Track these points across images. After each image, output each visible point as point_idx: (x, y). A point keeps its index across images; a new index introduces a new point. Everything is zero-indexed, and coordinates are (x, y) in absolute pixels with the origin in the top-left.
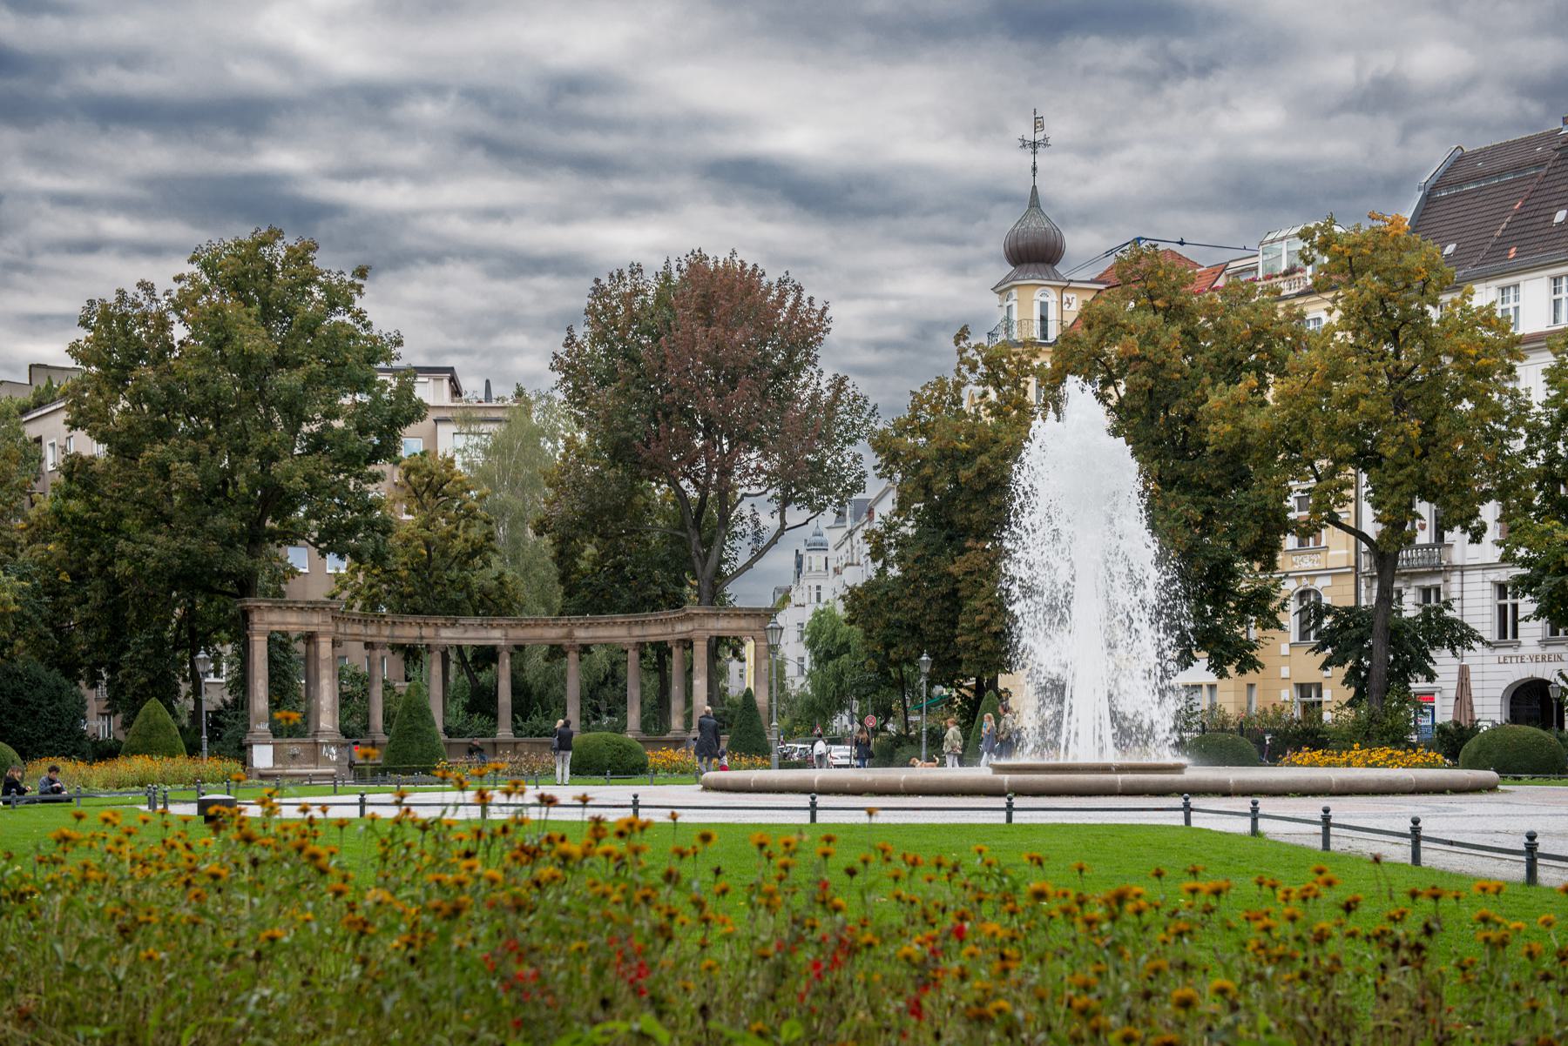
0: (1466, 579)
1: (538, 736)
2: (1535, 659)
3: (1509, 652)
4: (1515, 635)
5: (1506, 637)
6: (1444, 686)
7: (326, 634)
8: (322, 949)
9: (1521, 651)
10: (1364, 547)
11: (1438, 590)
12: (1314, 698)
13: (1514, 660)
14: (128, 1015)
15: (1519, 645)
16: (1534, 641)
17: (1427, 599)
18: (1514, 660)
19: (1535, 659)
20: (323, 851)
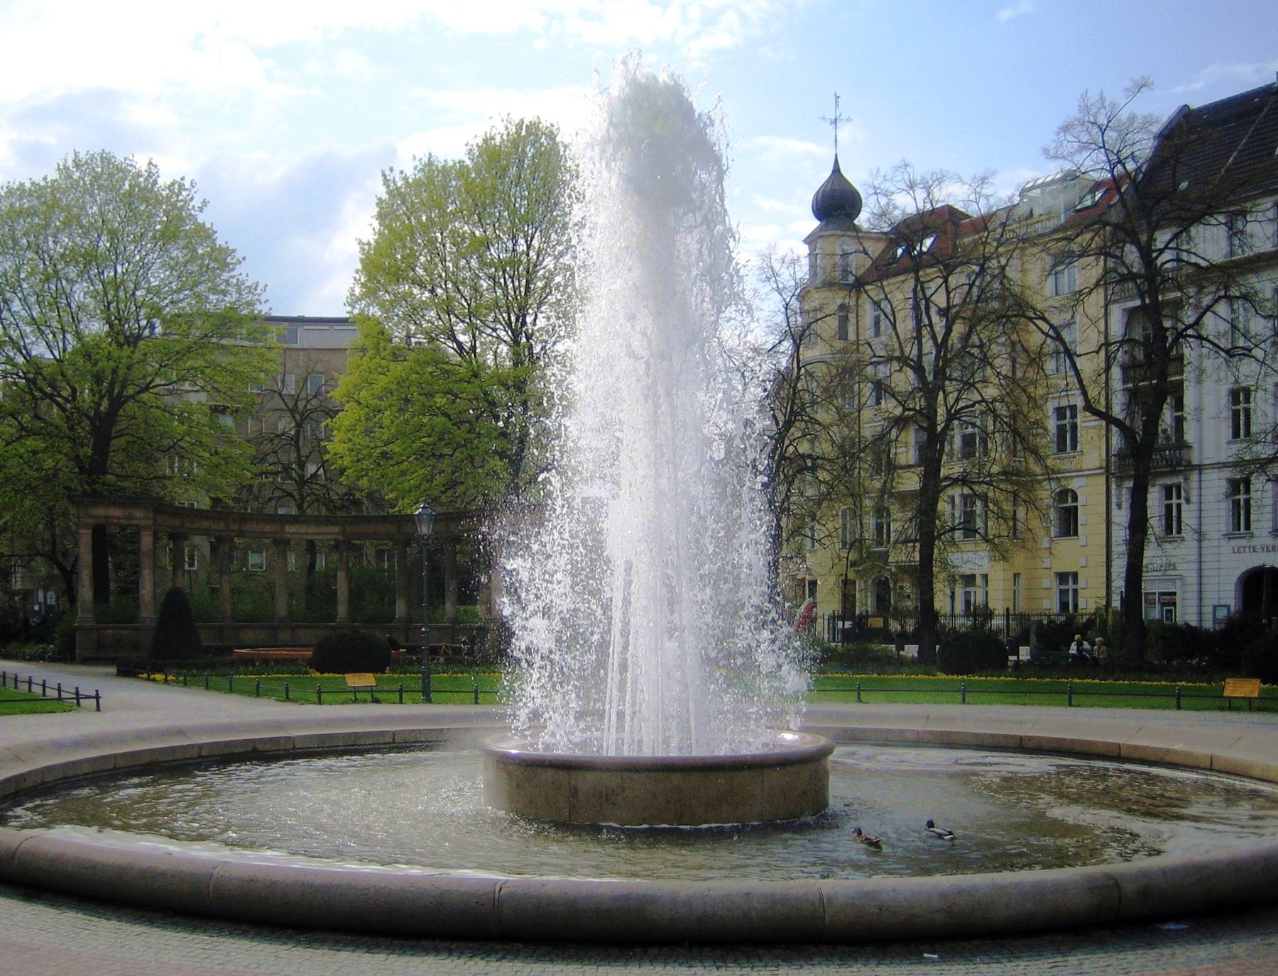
0: (1204, 477)
1: (231, 844)
2: (1267, 549)
3: (1243, 542)
4: (1248, 527)
5: (1239, 530)
6: (1184, 573)
7: (146, 528)
8: (354, 307)
9: (1254, 542)
10: (1114, 429)
11: (1179, 487)
12: (1070, 504)
13: (1247, 549)
14: (106, 493)
15: (1252, 536)
16: (1265, 533)
17: (1169, 497)
18: (1247, 549)
19: (1267, 549)
20: (413, 164)
